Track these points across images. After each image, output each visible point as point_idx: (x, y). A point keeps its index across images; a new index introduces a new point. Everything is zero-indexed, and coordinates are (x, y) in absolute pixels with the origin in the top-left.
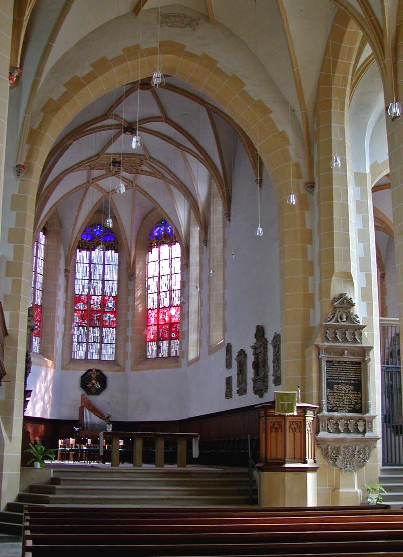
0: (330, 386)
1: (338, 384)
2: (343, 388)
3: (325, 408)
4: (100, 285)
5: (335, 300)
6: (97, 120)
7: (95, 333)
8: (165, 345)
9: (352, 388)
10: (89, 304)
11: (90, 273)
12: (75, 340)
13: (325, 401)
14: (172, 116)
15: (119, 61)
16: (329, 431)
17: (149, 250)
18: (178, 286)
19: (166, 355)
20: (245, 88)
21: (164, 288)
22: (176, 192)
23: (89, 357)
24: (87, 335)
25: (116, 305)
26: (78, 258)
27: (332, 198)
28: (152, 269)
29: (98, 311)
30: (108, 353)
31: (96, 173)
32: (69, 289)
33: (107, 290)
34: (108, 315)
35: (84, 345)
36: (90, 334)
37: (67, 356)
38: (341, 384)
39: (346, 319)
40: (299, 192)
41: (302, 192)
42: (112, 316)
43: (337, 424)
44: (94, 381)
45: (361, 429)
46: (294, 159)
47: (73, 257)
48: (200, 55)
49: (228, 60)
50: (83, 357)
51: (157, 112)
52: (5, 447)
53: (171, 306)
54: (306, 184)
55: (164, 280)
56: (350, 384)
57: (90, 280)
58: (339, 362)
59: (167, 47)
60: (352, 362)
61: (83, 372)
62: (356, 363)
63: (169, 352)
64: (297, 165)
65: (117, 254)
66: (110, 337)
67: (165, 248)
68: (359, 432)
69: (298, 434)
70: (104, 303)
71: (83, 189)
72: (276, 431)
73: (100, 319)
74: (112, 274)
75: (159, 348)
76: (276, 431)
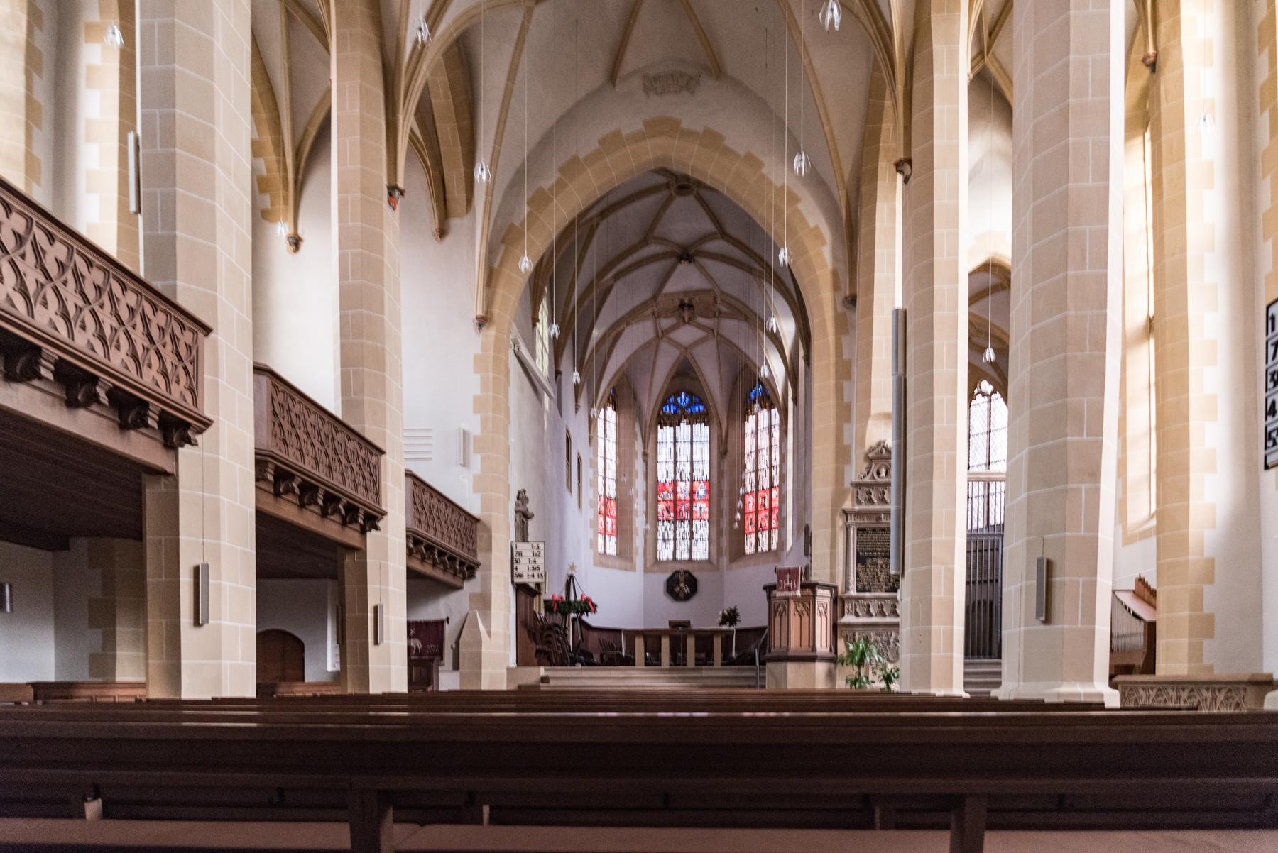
0: (861, 559)
1: (872, 557)
3: (853, 587)
4: (688, 469)
5: (871, 449)
7: (683, 528)
10: (675, 493)
12: (660, 537)
13: (852, 579)
14: (732, 230)
15: (593, 158)
16: (857, 615)
17: (745, 419)
20: (764, 171)
21: (763, 464)
25: (709, 491)
30: (701, 551)
31: (665, 323)
33: (697, 474)
34: (699, 504)
35: (672, 543)
37: (650, 557)
41: (840, 309)
48: (700, 130)
49: (740, 133)
50: (671, 557)
57: (675, 463)
58: (874, 530)
59: (658, 126)
61: (668, 575)
65: (707, 428)
69: (805, 618)
70: (692, 492)
71: (652, 347)
72: (781, 615)
73: (691, 511)
74: (702, 453)
75: (757, 539)
76: (781, 615)
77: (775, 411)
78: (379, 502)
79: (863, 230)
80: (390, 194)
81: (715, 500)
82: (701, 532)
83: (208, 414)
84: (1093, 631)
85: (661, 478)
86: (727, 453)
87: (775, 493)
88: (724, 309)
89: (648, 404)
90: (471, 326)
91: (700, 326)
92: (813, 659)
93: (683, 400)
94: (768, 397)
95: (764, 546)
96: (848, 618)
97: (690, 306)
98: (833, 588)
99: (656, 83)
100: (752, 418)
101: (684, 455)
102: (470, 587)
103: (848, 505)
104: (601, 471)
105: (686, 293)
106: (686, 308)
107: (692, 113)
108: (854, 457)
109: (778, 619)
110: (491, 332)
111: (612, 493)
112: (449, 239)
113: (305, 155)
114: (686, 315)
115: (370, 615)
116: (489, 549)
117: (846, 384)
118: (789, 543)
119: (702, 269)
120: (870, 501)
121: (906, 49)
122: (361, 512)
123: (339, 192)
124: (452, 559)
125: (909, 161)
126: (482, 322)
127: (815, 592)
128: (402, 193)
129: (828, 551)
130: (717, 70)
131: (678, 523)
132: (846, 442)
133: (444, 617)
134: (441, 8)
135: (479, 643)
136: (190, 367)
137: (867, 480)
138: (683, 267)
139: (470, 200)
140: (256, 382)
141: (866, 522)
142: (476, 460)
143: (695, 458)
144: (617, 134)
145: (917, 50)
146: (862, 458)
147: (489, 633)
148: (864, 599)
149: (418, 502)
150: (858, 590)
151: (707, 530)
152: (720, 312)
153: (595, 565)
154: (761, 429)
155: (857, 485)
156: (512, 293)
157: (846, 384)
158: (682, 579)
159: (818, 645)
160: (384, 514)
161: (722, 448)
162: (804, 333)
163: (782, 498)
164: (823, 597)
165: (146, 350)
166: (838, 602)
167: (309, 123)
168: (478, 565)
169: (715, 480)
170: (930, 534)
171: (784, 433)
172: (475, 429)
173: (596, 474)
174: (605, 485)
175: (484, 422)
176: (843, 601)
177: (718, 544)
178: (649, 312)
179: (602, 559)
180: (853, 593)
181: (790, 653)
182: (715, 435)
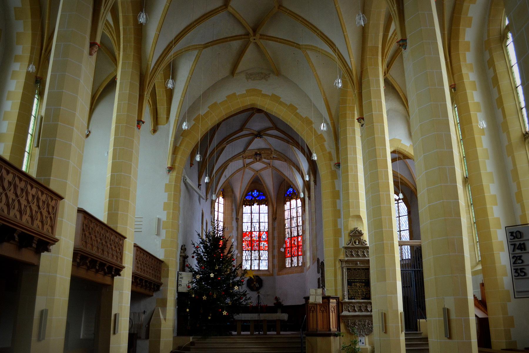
0: (349, 283)
1: (354, 282)
2: (358, 285)
3: (346, 297)
4: (257, 226)
5: (352, 231)
7: (255, 254)
10: (251, 237)
12: (244, 259)
13: (346, 293)
16: (349, 311)
19: (296, 265)
20: (298, 111)
21: (294, 225)
22: (295, 170)
23: (253, 269)
24: (251, 255)
25: (268, 237)
27: (347, 172)
28: (287, 214)
30: (264, 266)
31: (248, 161)
32: (239, 229)
33: (262, 228)
34: (263, 243)
35: (250, 261)
38: (357, 282)
40: (331, 168)
43: (354, 307)
44: (255, 283)
45: (369, 309)
46: (328, 150)
47: (241, 210)
50: (249, 269)
51: (270, 125)
52: (162, 325)
53: (298, 235)
54: (336, 164)
55: (294, 221)
56: (362, 282)
57: (251, 223)
58: (355, 269)
60: (363, 269)
62: (366, 269)
63: (298, 263)
64: (330, 153)
67: (293, 202)
68: (368, 311)
70: (260, 236)
72: (313, 312)
73: (259, 246)
74: (265, 218)
75: (292, 261)
76: (313, 312)
78: (122, 263)
79: (341, 137)
81: (271, 241)
82: (264, 256)
83: (57, 236)
84: (471, 342)
85: (245, 230)
86: (276, 218)
87: (300, 239)
89: (239, 191)
90: (165, 171)
91: (264, 163)
92: (329, 335)
93: (255, 193)
94: (295, 194)
95: (295, 264)
96: (345, 313)
98: (337, 298)
99: (251, 76)
100: (288, 203)
101: (255, 220)
103: (342, 257)
105: (259, 149)
107: (267, 87)
108: (343, 234)
109: (311, 314)
110: (174, 174)
112: (157, 133)
113: (96, 98)
114: (258, 158)
115: (113, 318)
116: (167, 277)
117: (338, 201)
118: (308, 265)
119: (266, 140)
120: (352, 256)
121: (358, 76)
122: (114, 269)
123: (116, 123)
125: (363, 119)
126: (171, 169)
127: (329, 301)
129: (333, 278)
131: (253, 252)
132: (339, 227)
134: (166, 54)
136: (52, 216)
137: (350, 246)
139: (168, 118)
140: (78, 216)
141: (351, 265)
142: (163, 232)
144: (234, 94)
145: (363, 79)
146: (347, 236)
147: (165, 319)
148: (351, 303)
150: (349, 299)
151: (267, 255)
154: (293, 208)
155: (346, 248)
156: (183, 157)
157: (338, 201)
159: (331, 327)
160: (124, 267)
161: (274, 217)
162: (313, 167)
163: (303, 241)
164: (333, 303)
165: (36, 212)
166: (340, 305)
167: (100, 86)
168: (161, 284)
169: (271, 231)
170: (348, 199)
171: (304, 211)
172: (164, 218)
175: (168, 214)
176: (342, 303)
177: (273, 263)
180: (347, 300)
181: (318, 332)
182: (271, 209)
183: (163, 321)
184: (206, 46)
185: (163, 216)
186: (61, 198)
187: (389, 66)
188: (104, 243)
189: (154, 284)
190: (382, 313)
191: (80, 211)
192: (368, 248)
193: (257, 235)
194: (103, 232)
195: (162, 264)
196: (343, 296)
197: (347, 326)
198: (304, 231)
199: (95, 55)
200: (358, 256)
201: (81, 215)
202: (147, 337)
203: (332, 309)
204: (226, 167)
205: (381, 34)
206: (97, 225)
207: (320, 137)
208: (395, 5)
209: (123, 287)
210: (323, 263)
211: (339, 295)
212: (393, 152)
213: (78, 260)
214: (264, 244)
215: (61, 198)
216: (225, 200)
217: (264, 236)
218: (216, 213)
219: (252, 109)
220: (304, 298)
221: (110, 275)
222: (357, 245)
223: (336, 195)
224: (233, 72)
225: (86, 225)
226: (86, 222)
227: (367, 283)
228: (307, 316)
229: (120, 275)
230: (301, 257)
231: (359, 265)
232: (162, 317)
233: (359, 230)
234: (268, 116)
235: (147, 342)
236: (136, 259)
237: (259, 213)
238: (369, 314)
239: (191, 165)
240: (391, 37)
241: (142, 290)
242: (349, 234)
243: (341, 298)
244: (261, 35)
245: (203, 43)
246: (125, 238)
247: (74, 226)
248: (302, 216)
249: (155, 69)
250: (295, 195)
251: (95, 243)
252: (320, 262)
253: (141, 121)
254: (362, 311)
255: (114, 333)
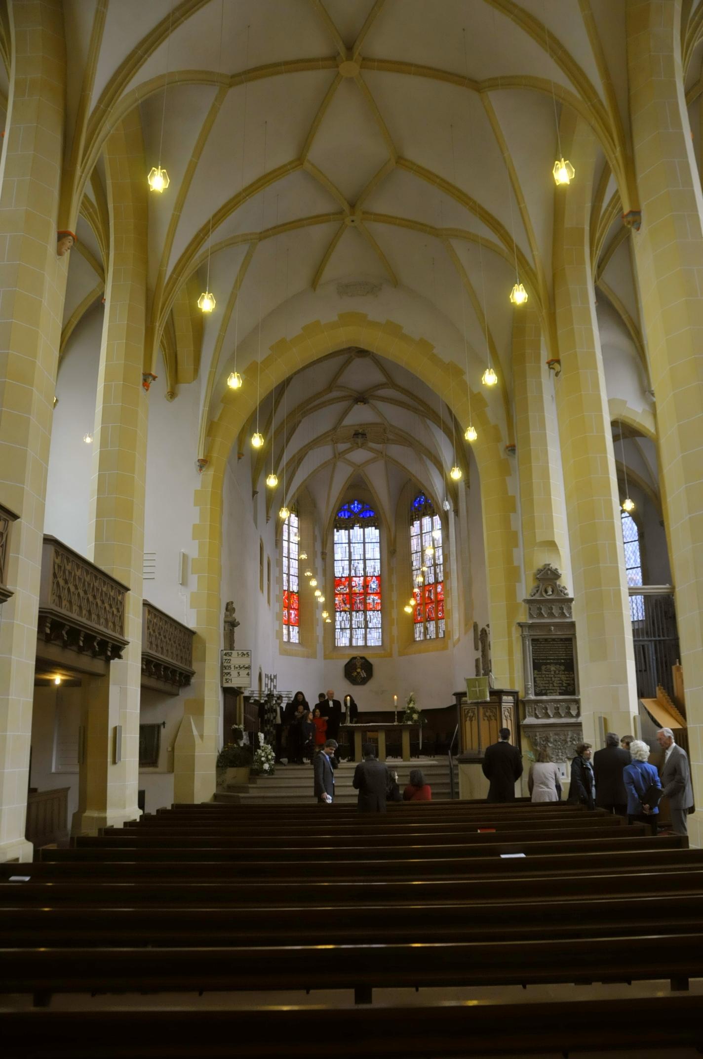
0: (537, 666)
1: (546, 664)
2: (553, 668)
3: (531, 691)
4: (361, 566)
5: (540, 571)
6: (319, 395)
7: (358, 618)
8: (432, 626)
9: (562, 668)
10: (351, 587)
11: (350, 553)
12: (338, 626)
13: (531, 684)
16: (537, 717)
18: (441, 561)
19: (433, 636)
20: (435, 351)
23: (354, 644)
24: (351, 620)
25: (380, 585)
26: (336, 538)
28: (415, 543)
29: (361, 594)
30: (375, 639)
31: (342, 447)
33: (370, 570)
34: (372, 597)
35: (348, 631)
36: (354, 618)
38: (550, 664)
39: (553, 592)
42: (376, 598)
43: (546, 709)
45: (574, 713)
50: (348, 644)
51: (379, 377)
53: (437, 582)
54: (507, 447)
56: (560, 664)
57: (350, 560)
58: (546, 640)
60: (561, 640)
61: (347, 660)
62: (567, 640)
63: (437, 633)
66: (375, 620)
67: (426, 520)
68: (572, 716)
70: (366, 586)
71: (330, 465)
72: (471, 721)
74: (374, 552)
76: (471, 721)
77: (437, 518)
78: (122, 632)
80: (145, 380)
85: (338, 574)
86: (396, 551)
88: (391, 437)
90: (193, 466)
91: (371, 450)
94: (430, 506)
96: (529, 720)
97: (364, 435)
98: (514, 694)
99: (346, 289)
100: (417, 524)
102: (185, 694)
103: (523, 618)
104: (285, 570)
106: (360, 436)
109: (468, 723)
110: (210, 472)
111: (294, 588)
113: (67, 338)
116: (203, 659)
120: (540, 615)
122: (110, 645)
123: (105, 380)
124: (174, 672)
125: (558, 361)
126: (203, 464)
128: (154, 378)
129: (507, 658)
130: (395, 282)
131: (354, 613)
132: (516, 564)
133: (160, 721)
135: (193, 746)
137: (537, 597)
138: (359, 407)
139: (196, 370)
141: (538, 634)
142: (193, 579)
143: (367, 556)
147: (202, 736)
149: (151, 626)
150: (536, 694)
151: (380, 619)
152: (388, 440)
153: (281, 654)
154: (428, 536)
155: (528, 602)
158: (358, 664)
160: (127, 643)
164: (508, 700)
166: (520, 705)
168: (193, 673)
173: (281, 572)
174: (288, 581)
176: (524, 703)
178: (329, 438)
179: (286, 648)
183: (198, 740)
184: (264, 235)
185: (193, 551)
186: (15, 517)
187: (600, 267)
188: (91, 599)
189: (181, 674)
190: (600, 718)
191: (50, 541)
192: (571, 600)
193: (361, 582)
194: (88, 579)
195: (194, 637)
196: (526, 689)
197: (533, 744)
198: (446, 574)
199: (67, 254)
200: (551, 615)
201: (51, 549)
202: (171, 769)
203: (507, 713)
204: (300, 460)
205: (588, 205)
206: (78, 566)
207: (478, 398)
208: (618, 149)
209: (126, 678)
210: (484, 633)
211: (518, 687)
212: (614, 424)
213: (48, 631)
214: (373, 599)
215: (15, 517)
216: (300, 520)
217: (374, 585)
218: (285, 544)
219: (349, 349)
220: (454, 694)
221: (103, 657)
222: (550, 595)
223: (509, 505)
224: (314, 283)
225: (59, 567)
226: (58, 561)
227: (570, 665)
228: (461, 727)
229: (120, 657)
230: (443, 621)
231: (553, 632)
232: (195, 732)
233: (554, 568)
234: (378, 362)
235: (171, 778)
236: (148, 628)
237: (364, 543)
238: (573, 720)
239: (240, 456)
240: (606, 210)
241: (160, 685)
242: (535, 575)
243: (521, 695)
244: (364, 213)
245: (259, 231)
246: (127, 589)
247: (39, 567)
248: (443, 547)
249: (174, 280)
250: (428, 508)
251: (75, 599)
252: (480, 629)
253: (150, 374)
254: (561, 717)
255: (114, 762)
